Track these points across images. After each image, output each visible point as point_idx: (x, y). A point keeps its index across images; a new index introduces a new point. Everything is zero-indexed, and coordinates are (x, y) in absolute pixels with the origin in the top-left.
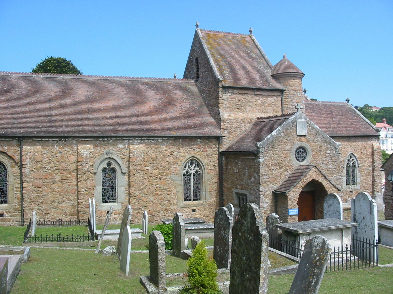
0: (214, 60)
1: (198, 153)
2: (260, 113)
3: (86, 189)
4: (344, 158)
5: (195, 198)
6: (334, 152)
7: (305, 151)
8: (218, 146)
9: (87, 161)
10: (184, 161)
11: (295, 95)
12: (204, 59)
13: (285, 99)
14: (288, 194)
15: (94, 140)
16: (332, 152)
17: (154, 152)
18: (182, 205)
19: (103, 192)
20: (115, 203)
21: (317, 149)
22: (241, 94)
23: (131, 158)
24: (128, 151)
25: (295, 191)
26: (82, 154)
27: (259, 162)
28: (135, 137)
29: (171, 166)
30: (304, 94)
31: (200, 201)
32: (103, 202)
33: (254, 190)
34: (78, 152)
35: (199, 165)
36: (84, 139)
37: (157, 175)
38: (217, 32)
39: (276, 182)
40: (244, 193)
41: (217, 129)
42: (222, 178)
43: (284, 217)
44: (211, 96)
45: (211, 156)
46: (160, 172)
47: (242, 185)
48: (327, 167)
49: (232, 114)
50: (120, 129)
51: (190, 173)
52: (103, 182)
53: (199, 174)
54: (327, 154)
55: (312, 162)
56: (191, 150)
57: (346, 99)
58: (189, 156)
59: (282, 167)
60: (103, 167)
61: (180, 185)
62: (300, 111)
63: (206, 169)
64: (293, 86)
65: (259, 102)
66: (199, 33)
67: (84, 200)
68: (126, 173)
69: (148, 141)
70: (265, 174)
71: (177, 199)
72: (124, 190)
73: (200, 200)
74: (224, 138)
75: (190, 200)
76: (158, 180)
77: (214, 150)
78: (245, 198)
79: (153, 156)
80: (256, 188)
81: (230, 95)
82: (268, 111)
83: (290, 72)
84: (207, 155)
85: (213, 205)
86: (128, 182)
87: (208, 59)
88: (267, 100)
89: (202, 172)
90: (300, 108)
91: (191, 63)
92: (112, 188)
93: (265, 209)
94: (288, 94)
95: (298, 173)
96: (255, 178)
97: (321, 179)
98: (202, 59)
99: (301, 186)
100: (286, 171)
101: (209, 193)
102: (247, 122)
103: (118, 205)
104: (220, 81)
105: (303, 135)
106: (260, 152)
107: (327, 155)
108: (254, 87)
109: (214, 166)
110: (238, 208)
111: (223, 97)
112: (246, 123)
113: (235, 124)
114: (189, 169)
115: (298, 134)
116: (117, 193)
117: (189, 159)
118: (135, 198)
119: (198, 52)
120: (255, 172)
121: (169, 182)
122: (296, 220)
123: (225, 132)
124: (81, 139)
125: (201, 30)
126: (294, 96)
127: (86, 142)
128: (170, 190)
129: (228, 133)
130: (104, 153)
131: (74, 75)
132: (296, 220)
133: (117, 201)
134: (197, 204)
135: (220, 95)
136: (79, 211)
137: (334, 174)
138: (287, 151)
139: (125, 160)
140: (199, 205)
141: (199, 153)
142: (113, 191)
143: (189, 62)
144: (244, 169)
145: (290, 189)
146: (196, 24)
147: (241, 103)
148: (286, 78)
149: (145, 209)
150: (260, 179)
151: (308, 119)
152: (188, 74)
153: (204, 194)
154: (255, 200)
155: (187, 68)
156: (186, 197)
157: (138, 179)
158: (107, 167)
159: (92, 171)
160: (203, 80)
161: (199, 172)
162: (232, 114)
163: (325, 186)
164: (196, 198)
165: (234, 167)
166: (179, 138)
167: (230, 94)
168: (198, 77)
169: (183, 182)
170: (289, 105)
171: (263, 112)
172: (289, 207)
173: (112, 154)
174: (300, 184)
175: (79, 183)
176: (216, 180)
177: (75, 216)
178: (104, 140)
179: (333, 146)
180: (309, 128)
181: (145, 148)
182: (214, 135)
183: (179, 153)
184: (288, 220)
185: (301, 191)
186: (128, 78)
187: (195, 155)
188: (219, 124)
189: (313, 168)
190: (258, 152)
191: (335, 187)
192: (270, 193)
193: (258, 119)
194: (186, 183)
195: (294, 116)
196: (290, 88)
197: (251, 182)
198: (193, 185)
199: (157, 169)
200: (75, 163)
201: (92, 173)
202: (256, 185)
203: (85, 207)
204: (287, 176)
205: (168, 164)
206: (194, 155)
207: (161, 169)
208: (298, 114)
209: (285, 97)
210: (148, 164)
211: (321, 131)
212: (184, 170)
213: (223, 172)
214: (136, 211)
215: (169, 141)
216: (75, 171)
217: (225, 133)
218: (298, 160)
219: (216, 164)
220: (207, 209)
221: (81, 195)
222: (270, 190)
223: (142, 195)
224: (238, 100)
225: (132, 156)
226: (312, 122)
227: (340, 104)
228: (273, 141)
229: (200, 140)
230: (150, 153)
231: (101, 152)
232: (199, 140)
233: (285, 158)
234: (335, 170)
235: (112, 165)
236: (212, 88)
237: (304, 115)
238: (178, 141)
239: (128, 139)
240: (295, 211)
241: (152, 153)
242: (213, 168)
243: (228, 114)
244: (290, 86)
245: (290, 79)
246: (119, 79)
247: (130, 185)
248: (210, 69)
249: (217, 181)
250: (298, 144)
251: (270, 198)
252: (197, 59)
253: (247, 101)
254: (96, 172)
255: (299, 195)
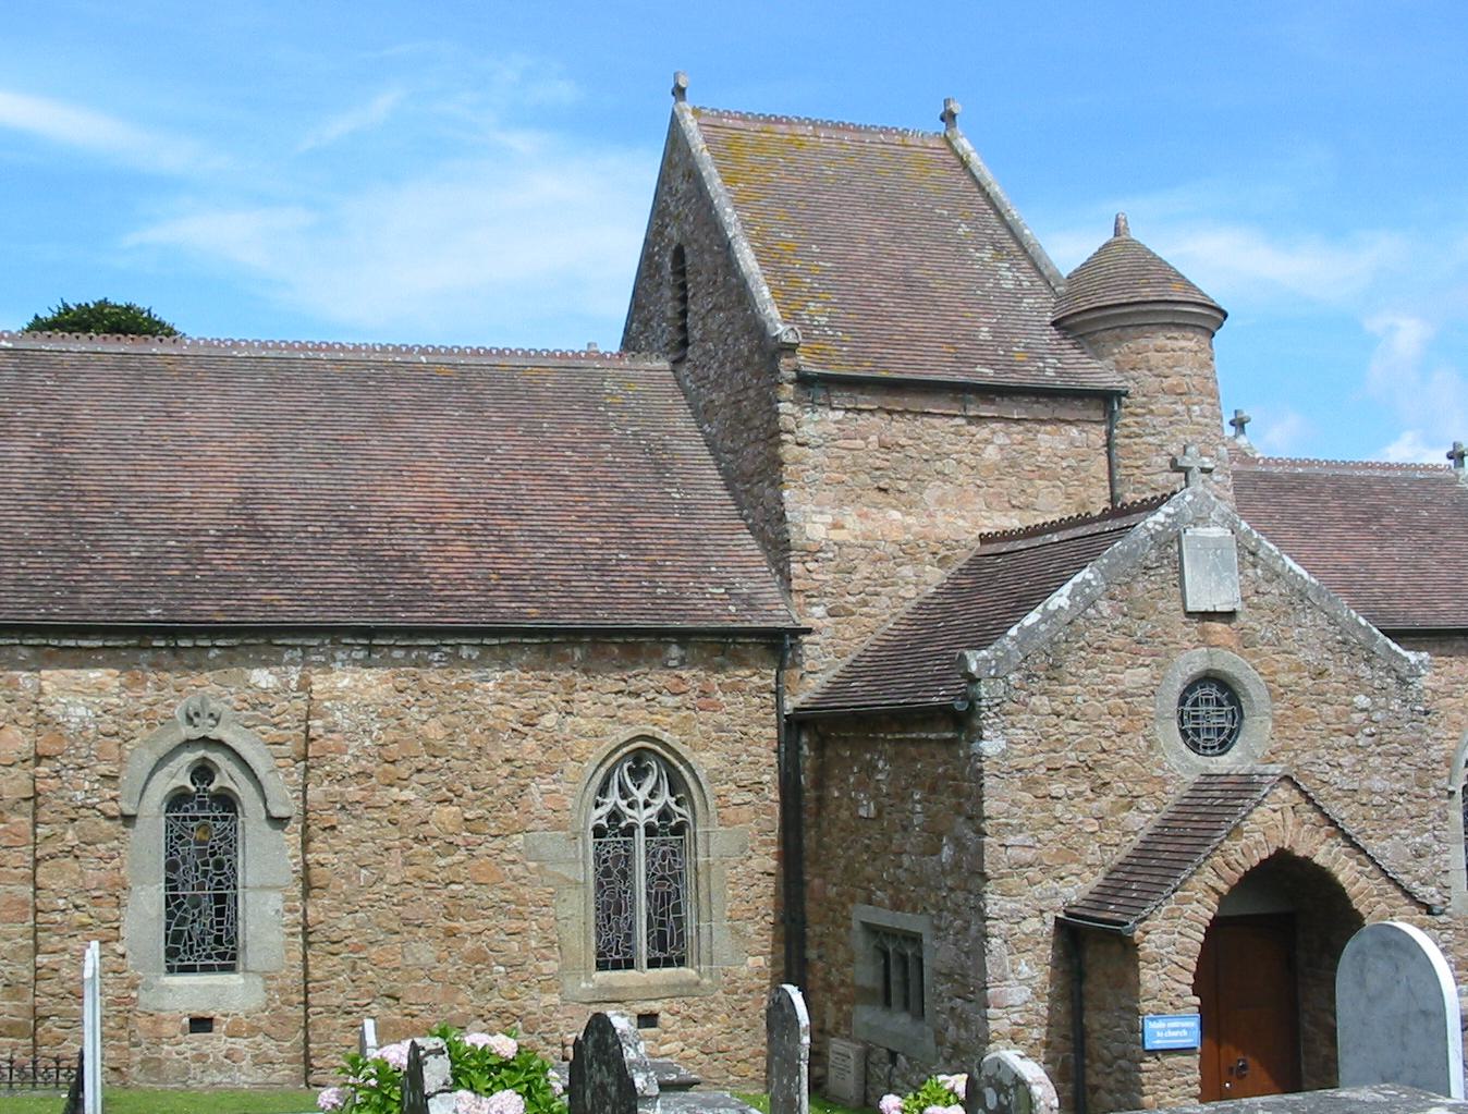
0: (758, 253)
1: (670, 720)
2: (996, 514)
3: (78, 902)
4: (1452, 744)
5: (658, 954)
6: (1395, 705)
7: (1234, 699)
8: (778, 682)
9: (84, 752)
10: (595, 758)
11: (1176, 417)
12: (711, 251)
13: (1127, 441)
14: (1138, 933)
15: (127, 647)
16: (1382, 702)
17: (436, 713)
18: (584, 990)
19: (170, 915)
20: (233, 976)
21: (1297, 684)
22: (895, 416)
23: (313, 740)
24: (301, 704)
25: (1177, 914)
26: (61, 719)
27: (979, 757)
28: (334, 632)
29: (527, 785)
30: (1236, 436)
31: (682, 969)
32: (171, 970)
33: (956, 912)
34: (42, 707)
35: (676, 785)
36: (72, 643)
37: (451, 829)
38: (778, 121)
39: (1075, 867)
40: (905, 928)
41: (771, 592)
42: (799, 849)
43: (1122, 1062)
44: (742, 431)
45: (738, 735)
46: (467, 815)
47: (895, 883)
48: (1355, 785)
49: (849, 519)
50: (261, 593)
51: (630, 820)
52: (172, 866)
53: (679, 829)
54: (1354, 716)
55: (1273, 758)
56: (633, 701)
57: (1451, 449)
58: (624, 734)
59: (1105, 784)
60: (169, 788)
61: (577, 883)
62: (1198, 483)
63: (712, 803)
64: (1167, 372)
65: (991, 453)
66: (690, 123)
67: (67, 957)
68: (289, 818)
69: (408, 655)
70: (1015, 822)
71: (557, 956)
72: (280, 906)
73: (681, 962)
74: (806, 639)
75: (630, 965)
76: (456, 858)
77: (756, 701)
78: (913, 954)
79: (435, 731)
80: (966, 899)
81: (836, 422)
82: (1041, 502)
83: (1151, 299)
84: (720, 728)
85: (750, 992)
86: (298, 868)
87: (727, 247)
88: (1031, 444)
89: (694, 820)
90: (1196, 470)
91: (652, 277)
92: (220, 899)
93: (1016, 1017)
94: (1144, 415)
95: (1196, 818)
96: (959, 844)
97: (1324, 848)
98: (702, 251)
99: (1214, 889)
100: (1129, 807)
101: (732, 928)
102: (928, 557)
103: (245, 986)
104: (783, 349)
105: (1218, 609)
106: (984, 703)
107: (1357, 717)
108: (961, 378)
109: (757, 787)
110: (879, 1009)
111: (804, 428)
112: (921, 562)
113: (865, 569)
114: (625, 802)
115: (1190, 608)
116: (240, 923)
117: (625, 750)
118: (333, 948)
119: (683, 216)
120: (959, 814)
121: (517, 870)
122: (1187, 1078)
123: (814, 609)
124: (56, 643)
125: (696, 112)
126: (1173, 419)
127: (82, 659)
128: (521, 908)
129: (831, 613)
130: (179, 713)
131: (63, 336)
132: (1187, 1078)
133: (241, 967)
134: (668, 986)
135: (786, 421)
136: (41, 1011)
137: (1396, 823)
138: (1132, 695)
139: (286, 749)
140: (675, 993)
141: (675, 718)
142: (220, 912)
143: (645, 274)
144: (903, 796)
145: (1151, 906)
146: (673, 86)
147: (898, 461)
148: (1130, 330)
149: (388, 1006)
150: (988, 851)
151: (1244, 525)
152: (641, 333)
153: (704, 931)
154: (962, 967)
155: (637, 305)
156: (610, 950)
157: (352, 849)
158: (193, 789)
159: (112, 809)
160: (706, 353)
161: (679, 819)
162: (849, 519)
163: (1351, 891)
164: (663, 955)
165: (858, 791)
166: (572, 638)
167: (840, 415)
168: (685, 344)
169: (591, 871)
170: (1148, 470)
171: (1014, 507)
172: (1144, 1006)
173: (217, 720)
174: (1208, 875)
175: (40, 870)
176: (766, 860)
177: (22, 1041)
178: (175, 650)
179: (1390, 670)
180: (1250, 572)
181: (389, 690)
182: (755, 624)
183: (569, 719)
184: (1144, 1077)
185: (1211, 915)
186: (330, 347)
187: (656, 729)
188: (780, 571)
189: (1273, 787)
190: (973, 702)
191: (1408, 894)
192: (1040, 927)
193: (985, 539)
194: (607, 873)
195: (1165, 508)
196: (1151, 382)
197: (939, 869)
198: (643, 884)
199: (451, 801)
200: (28, 763)
201: (112, 818)
202: (966, 881)
203: (70, 993)
204: (1136, 833)
205: (512, 774)
206: (650, 730)
207: (472, 801)
208: (1189, 498)
209: (1126, 431)
210: (406, 777)
211: (1318, 589)
212: (597, 806)
213: (805, 816)
214: (341, 1021)
215: (514, 656)
216: (28, 807)
217: (812, 615)
218: (1194, 747)
219: (766, 778)
220: (718, 1013)
221: (49, 929)
222: (1042, 912)
223: (369, 932)
224: (883, 445)
225: (321, 731)
226: (1265, 542)
227: (1418, 475)
228: (1053, 644)
229: (683, 653)
230: (417, 716)
231: (160, 709)
232: (675, 651)
233: (1121, 733)
234: (1401, 800)
235: (217, 778)
236: (747, 388)
237: (1226, 507)
238: (564, 658)
239: (299, 642)
240: (1180, 1029)
241: (425, 717)
242: (749, 797)
243: (829, 519)
244: (1150, 370)
245: (1120, 339)
246: (285, 353)
247: (309, 884)
248: (740, 293)
249: (772, 864)
250: (1194, 661)
251: (1040, 957)
252: (679, 254)
253: (926, 452)
254: (132, 812)
255: (1202, 938)
